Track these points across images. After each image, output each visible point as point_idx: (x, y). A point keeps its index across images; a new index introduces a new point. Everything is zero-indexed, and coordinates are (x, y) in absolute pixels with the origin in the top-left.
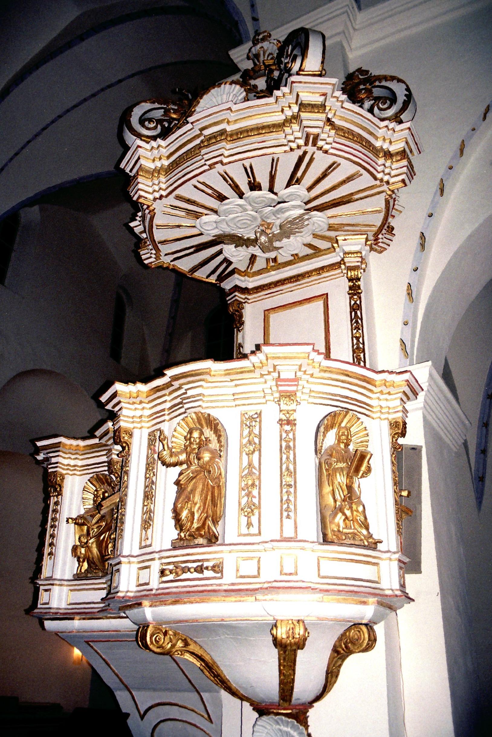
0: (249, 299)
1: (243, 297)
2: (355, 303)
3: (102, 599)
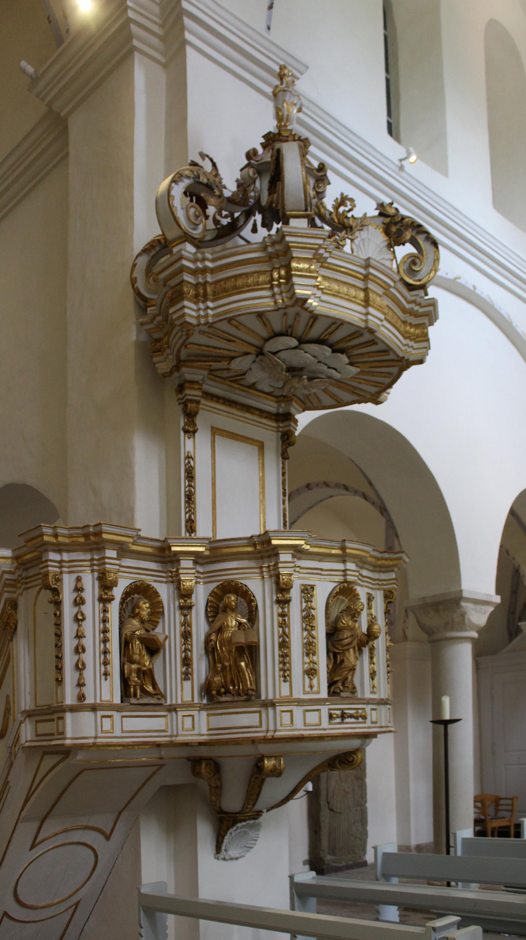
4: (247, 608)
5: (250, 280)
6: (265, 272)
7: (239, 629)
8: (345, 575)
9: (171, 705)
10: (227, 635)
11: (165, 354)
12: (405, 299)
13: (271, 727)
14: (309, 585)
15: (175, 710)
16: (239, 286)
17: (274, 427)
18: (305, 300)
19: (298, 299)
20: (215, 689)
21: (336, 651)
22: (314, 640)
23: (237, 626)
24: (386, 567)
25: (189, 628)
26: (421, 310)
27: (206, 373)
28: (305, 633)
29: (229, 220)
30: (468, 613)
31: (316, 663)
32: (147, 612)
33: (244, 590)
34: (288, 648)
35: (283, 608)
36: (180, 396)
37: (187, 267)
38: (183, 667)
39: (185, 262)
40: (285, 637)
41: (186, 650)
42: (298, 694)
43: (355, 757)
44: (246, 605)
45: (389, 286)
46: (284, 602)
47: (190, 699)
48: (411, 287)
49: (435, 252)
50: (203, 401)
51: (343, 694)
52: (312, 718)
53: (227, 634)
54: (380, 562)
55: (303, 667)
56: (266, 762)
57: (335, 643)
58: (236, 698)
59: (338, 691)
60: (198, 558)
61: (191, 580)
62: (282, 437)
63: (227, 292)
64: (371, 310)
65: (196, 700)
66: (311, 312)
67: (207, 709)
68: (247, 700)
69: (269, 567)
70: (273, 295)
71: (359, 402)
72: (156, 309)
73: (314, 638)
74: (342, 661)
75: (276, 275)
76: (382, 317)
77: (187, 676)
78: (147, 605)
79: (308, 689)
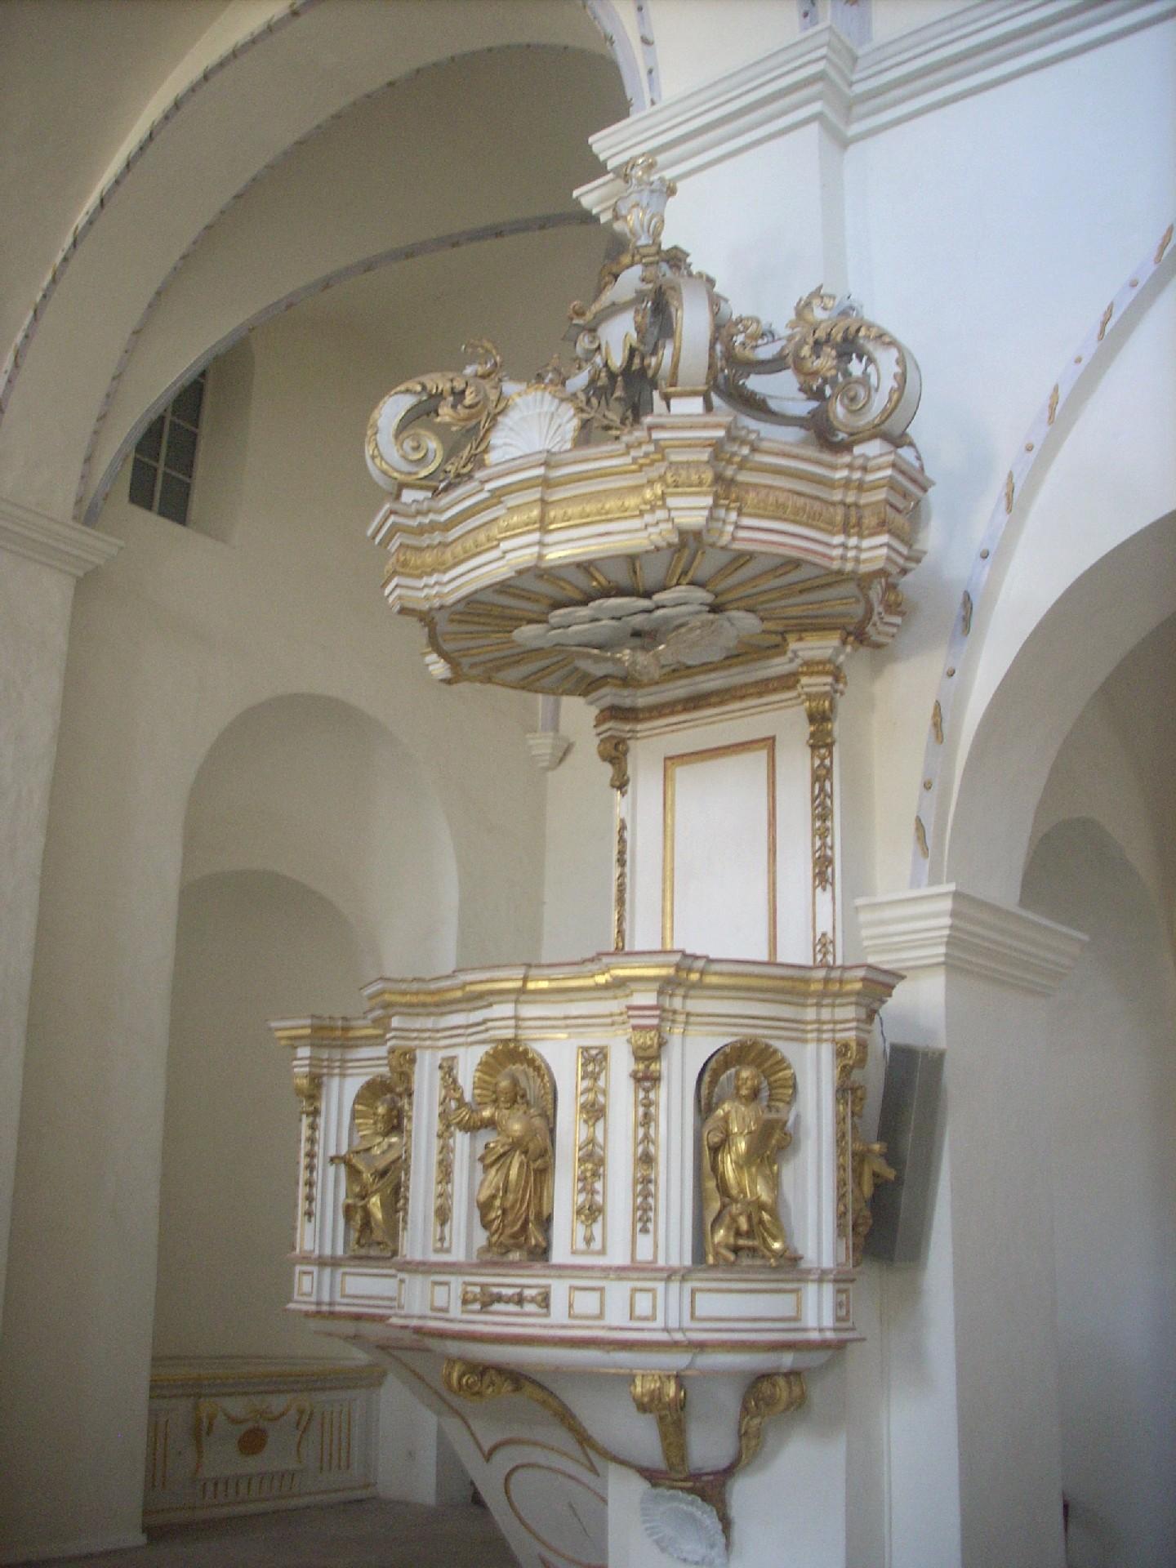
0: (637, 732)
1: (628, 727)
2: (822, 765)
3: (671, 191)
52: (440, 1296)
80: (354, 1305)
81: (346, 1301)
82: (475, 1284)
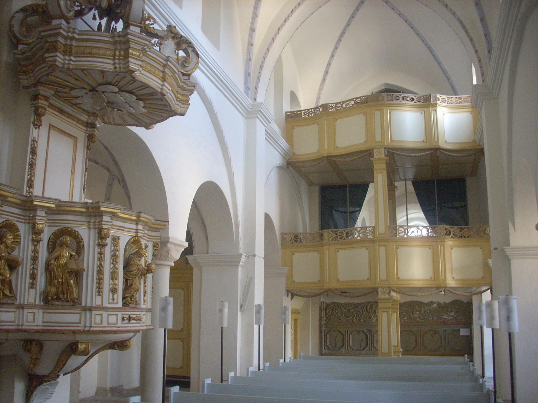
4: (76, 246)
5: (101, 52)
6: (110, 50)
7: (70, 259)
8: (137, 232)
9: (20, 304)
10: (63, 261)
11: (28, 76)
12: (180, 80)
13: (88, 324)
14: (116, 236)
15: (23, 308)
16: (93, 53)
17: (84, 130)
18: (133, 72)
19: (130, 70)
20: (51, 296)
21: (128, 278)
22: (117, 271)
23: (69, 256)
24: (156, 228)
25: (37, 254)
26: (187, 88)
27: (53, 93)
28: (112, 266)
29: (79, 8)
30: (171, 251)
31: (117, 285)
32: (11, 242)
33: (76, 234)
34: (102, 274)
35: (101, 249)
36: (33, 102)
37: (61, 33)
38: (31, 279)
39: (61, 31)
40: (101, 267)
41: (34, 268)
42: (106, 305)
43: (128, 343)
44: (75, 243)
45: (176, 73)
46: (102, 246)
47: (33, 301)
48: (184, 75)
49: (197, 59)
50: (48, 109)
51: (131, 305)
52: (112, 319)
53: (63, 261)
54: (153, 226)
55: (109, 287)
56: (80, 346)
57: (127, 273)
58: (65, 303)
59: (128, 303)
60: (49, 211)
61: (43, 224)
62: (88, 136)
63: (85, 54)
64: (166, 84)
65: (37, 303)
66: (134, 78)
67: (43, 309)
68: (73, 305)
69: (95, 222)
70: (114, 64)
71: (137, 126)
72: (27, 48)
73: (117, 269)
74: (131, 285)
75: (117, 53)
76: (170, 88)
77: (32, 286)
78: (12, 237)
79: (111, 301)
80: (47, 326)
81: (28, 324)
82: (126, 314)
